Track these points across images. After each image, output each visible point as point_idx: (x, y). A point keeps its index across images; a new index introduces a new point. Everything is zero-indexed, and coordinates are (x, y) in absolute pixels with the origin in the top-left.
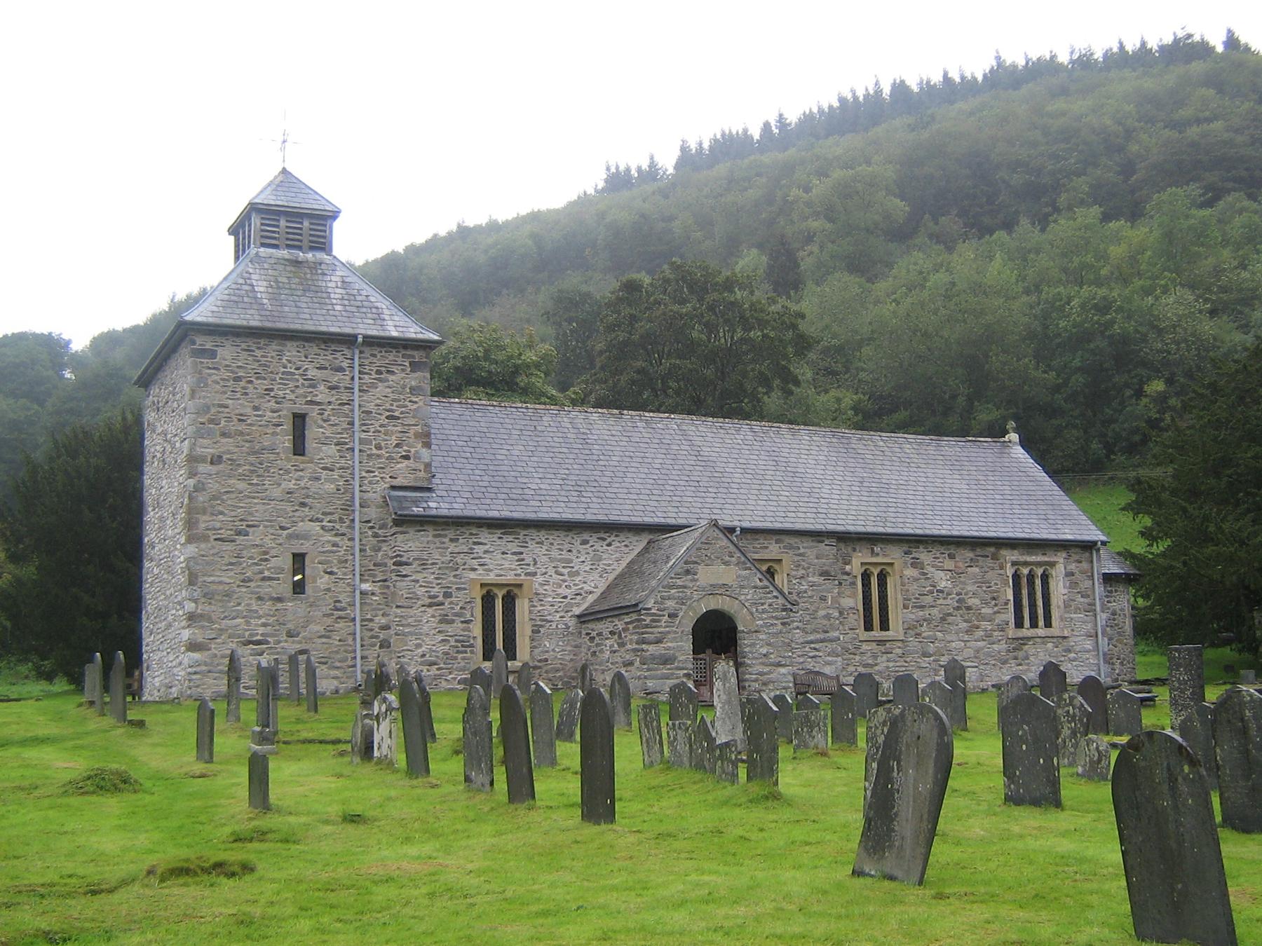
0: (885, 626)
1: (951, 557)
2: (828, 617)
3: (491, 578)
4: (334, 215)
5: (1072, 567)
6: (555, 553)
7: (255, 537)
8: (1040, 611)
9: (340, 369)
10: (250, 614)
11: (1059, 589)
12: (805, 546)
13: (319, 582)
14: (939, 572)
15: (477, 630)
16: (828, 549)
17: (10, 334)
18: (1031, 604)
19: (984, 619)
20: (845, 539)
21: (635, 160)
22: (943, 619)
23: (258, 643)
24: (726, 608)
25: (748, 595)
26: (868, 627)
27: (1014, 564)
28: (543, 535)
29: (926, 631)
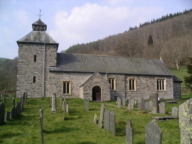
3: (65, 80)
8: (162, 87)
10: (26, 86)
14: (143, 80)
15: (62, 89)
16: (123, 76)
19: (151, 88)
21: (133, 26)
22: (144, 88)
23: (28, 90)
24: (98, 86)
27: (157, 79)
29: (141, 90)
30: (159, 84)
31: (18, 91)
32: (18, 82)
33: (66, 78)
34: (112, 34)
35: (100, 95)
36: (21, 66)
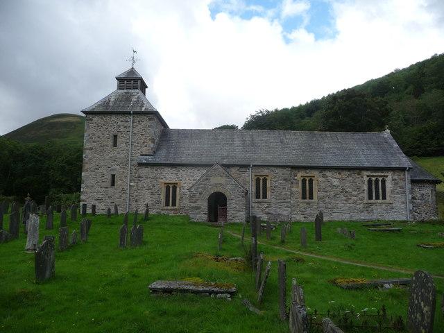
0: (311, 197)
1: (340, 174)
2: (286, 194)
3: (167, 181)
4: (132, 82)
5: (396, 177)
6: (188, 174)
7: (100, 170)
9: (128, 122)
11: (389, 186)
12: (277, 170)
13: (118, 182)
14: (334, 179)
16: (287, 171)
17: (280, 109)
18: (376, 190)
20: (294, 168)
22: (335, 196)
25: (230, 187)
26: (304, 197)
27: (368, 176)
28: (184, 168)
30: (373, 186)
31: (83, 201)
32: (83, 185)
33: (169, 176)
34: (368, 80)
35: (225, 211)
36: (90, 156)
